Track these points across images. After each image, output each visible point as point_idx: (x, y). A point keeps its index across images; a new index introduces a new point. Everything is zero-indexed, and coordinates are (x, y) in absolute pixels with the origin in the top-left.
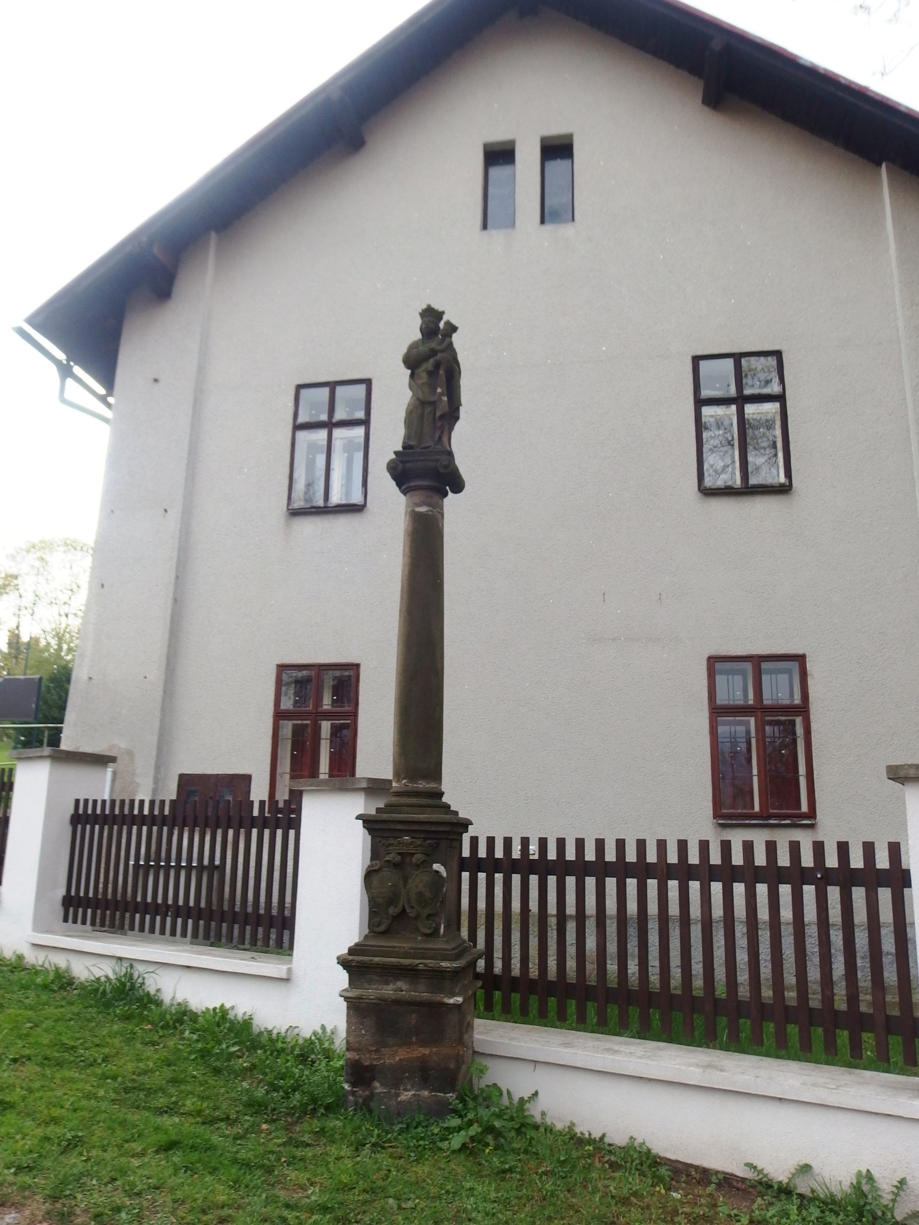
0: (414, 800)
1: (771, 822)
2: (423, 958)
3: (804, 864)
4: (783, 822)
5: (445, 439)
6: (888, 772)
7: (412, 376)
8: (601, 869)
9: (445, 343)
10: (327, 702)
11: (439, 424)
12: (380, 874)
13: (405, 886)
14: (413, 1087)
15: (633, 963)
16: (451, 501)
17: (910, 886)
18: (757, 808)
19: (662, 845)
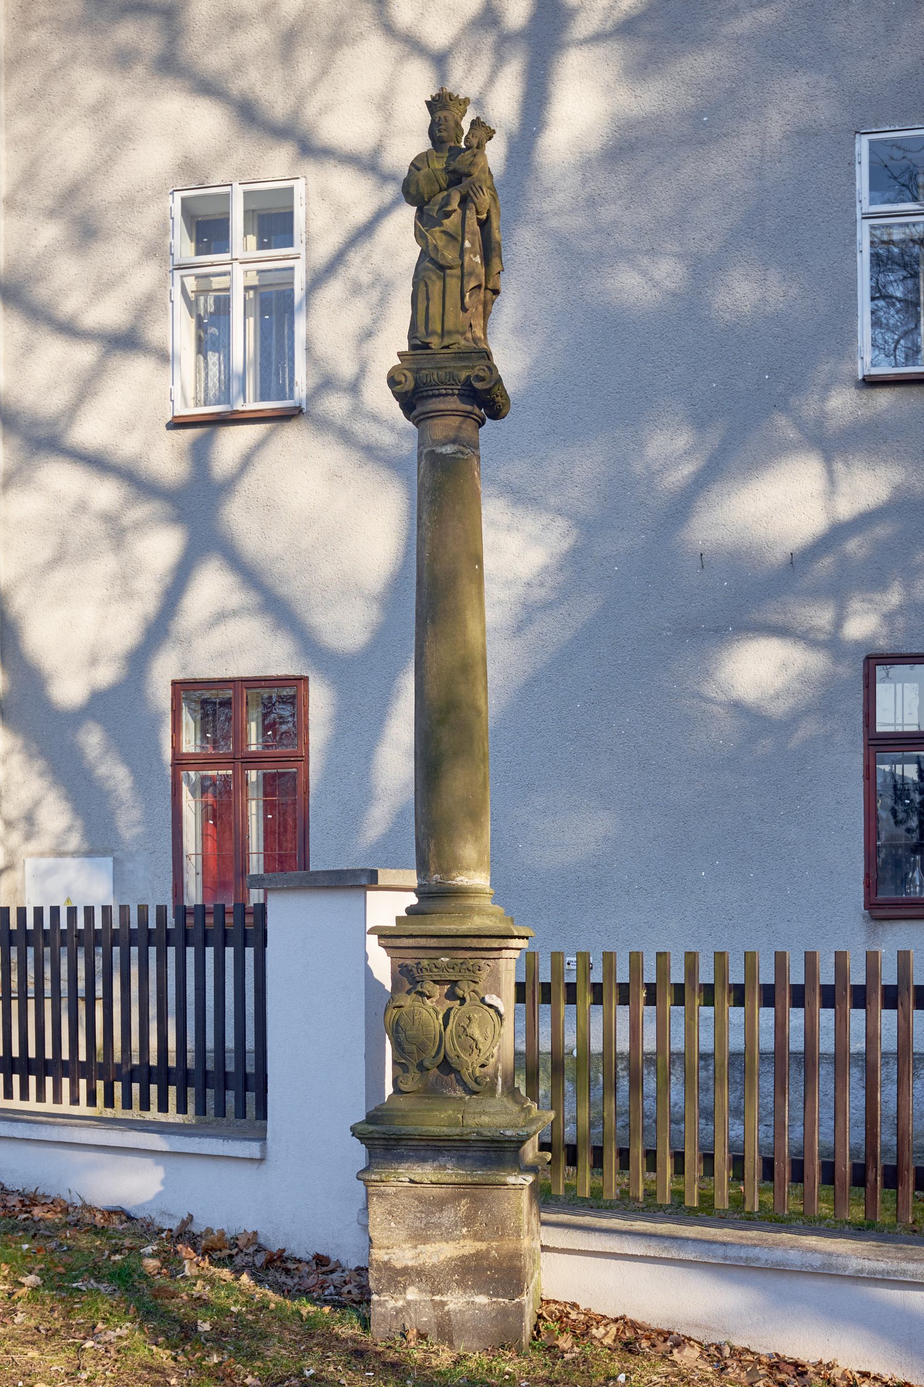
10: (254, 741)
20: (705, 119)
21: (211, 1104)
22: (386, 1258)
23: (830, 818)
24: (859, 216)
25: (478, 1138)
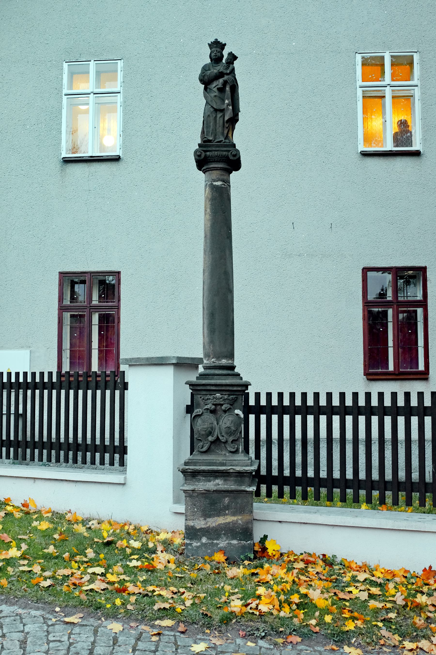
0: (221, 372)
2: (231, 465)
3: (412, 405)
5: (230, 135)
7: (206, 89)
8: (293, 410)
9: (231, 68)
11: (227, 125)
12: (202, 417)
13: (218, 424)
14: (227, 539)
15: (311, 469)
16: (234, 176)
18: (391, 368)
19: (292, 395)
20: (294, 44)
21: (79, 458)
22: (192, 524)
23: (349, 336)
24: (358, 87)
25: (233, 471)
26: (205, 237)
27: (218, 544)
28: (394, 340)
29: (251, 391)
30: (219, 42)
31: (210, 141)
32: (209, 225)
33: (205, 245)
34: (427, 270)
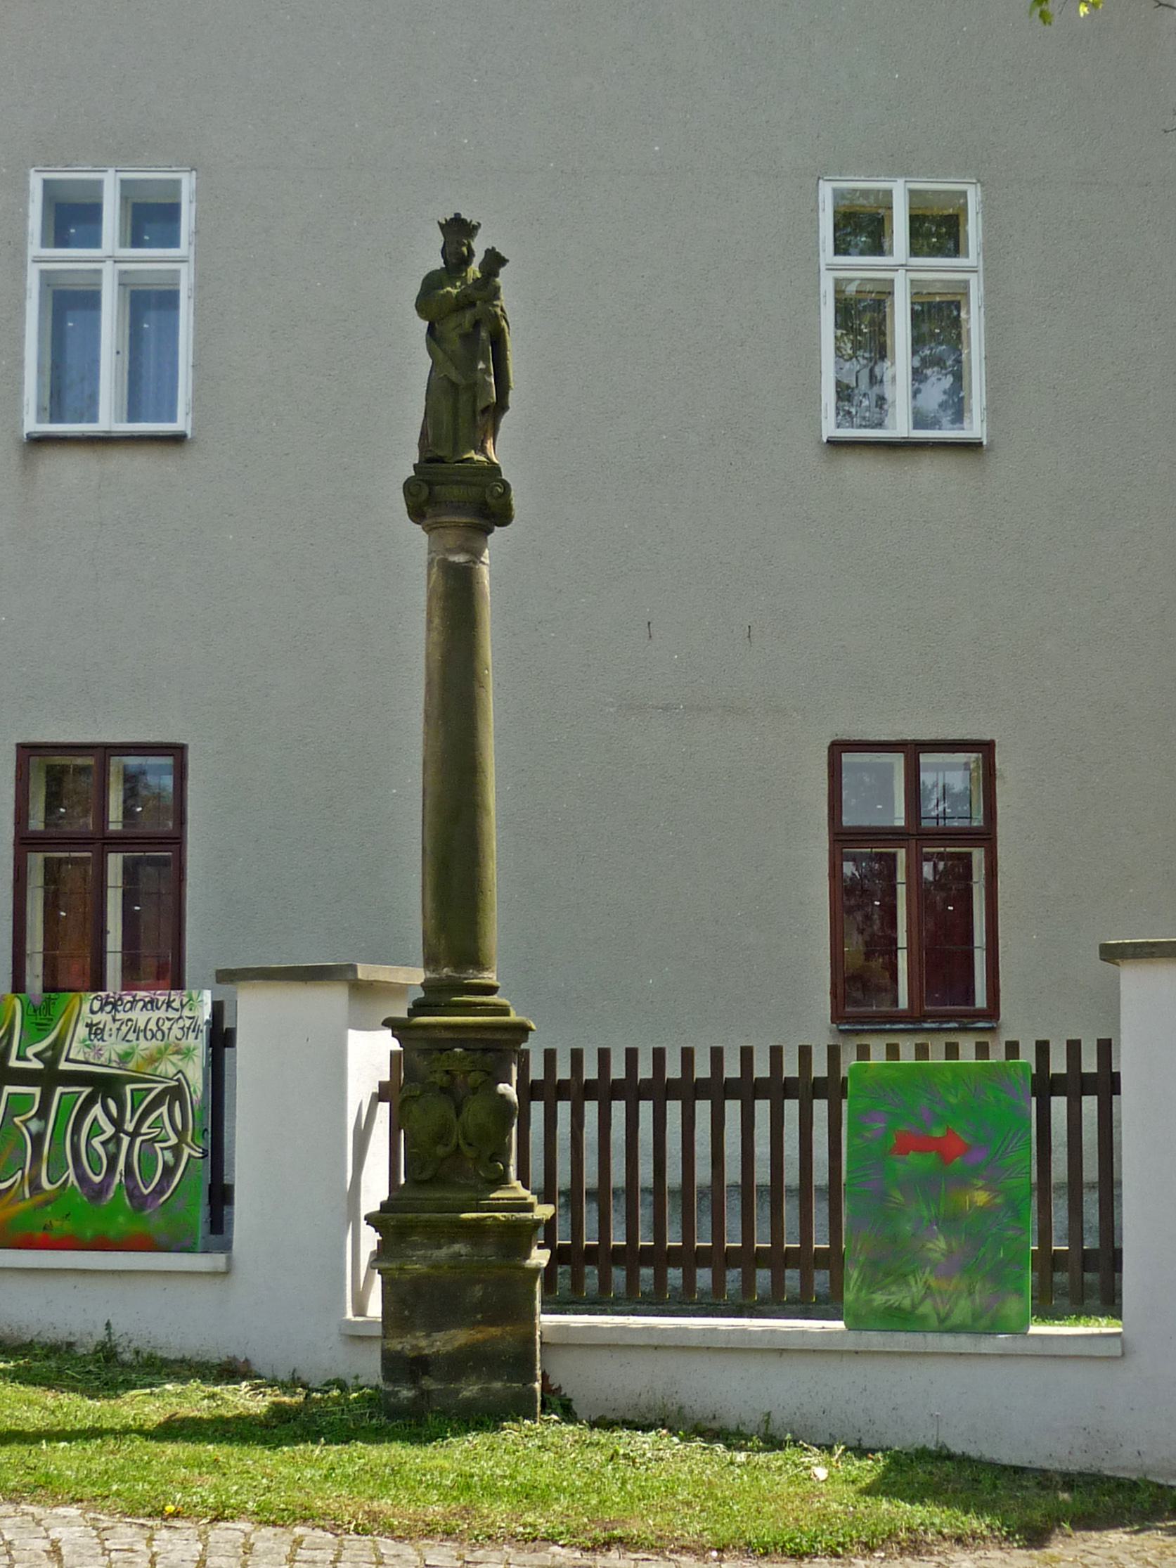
1: (926, 1025)
4: (945, 1026)
6: (1101, 952)
17: (1119, 1093)
18: (903, 1003)
22: (399, 1347)
26: (428, 684)
27: (458, 1392)
28: (909, 931)
29: (534, 1047)
30: (464, 221)
31: (440, 460)
32: (437, 657)
33: (428, 703)
34: (997, 750)
